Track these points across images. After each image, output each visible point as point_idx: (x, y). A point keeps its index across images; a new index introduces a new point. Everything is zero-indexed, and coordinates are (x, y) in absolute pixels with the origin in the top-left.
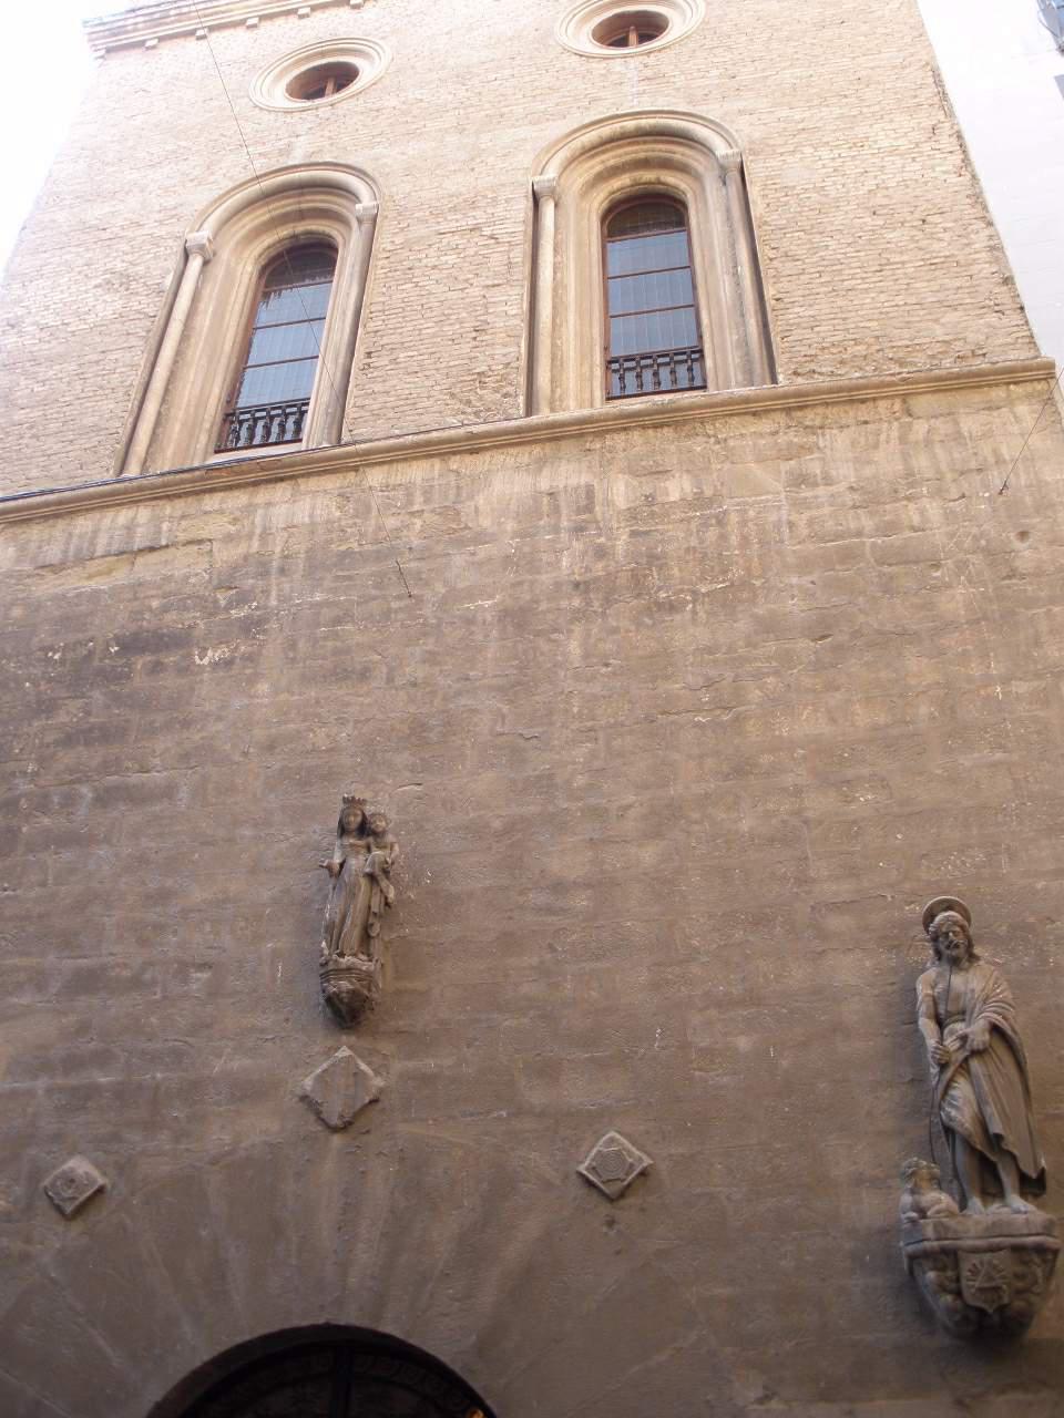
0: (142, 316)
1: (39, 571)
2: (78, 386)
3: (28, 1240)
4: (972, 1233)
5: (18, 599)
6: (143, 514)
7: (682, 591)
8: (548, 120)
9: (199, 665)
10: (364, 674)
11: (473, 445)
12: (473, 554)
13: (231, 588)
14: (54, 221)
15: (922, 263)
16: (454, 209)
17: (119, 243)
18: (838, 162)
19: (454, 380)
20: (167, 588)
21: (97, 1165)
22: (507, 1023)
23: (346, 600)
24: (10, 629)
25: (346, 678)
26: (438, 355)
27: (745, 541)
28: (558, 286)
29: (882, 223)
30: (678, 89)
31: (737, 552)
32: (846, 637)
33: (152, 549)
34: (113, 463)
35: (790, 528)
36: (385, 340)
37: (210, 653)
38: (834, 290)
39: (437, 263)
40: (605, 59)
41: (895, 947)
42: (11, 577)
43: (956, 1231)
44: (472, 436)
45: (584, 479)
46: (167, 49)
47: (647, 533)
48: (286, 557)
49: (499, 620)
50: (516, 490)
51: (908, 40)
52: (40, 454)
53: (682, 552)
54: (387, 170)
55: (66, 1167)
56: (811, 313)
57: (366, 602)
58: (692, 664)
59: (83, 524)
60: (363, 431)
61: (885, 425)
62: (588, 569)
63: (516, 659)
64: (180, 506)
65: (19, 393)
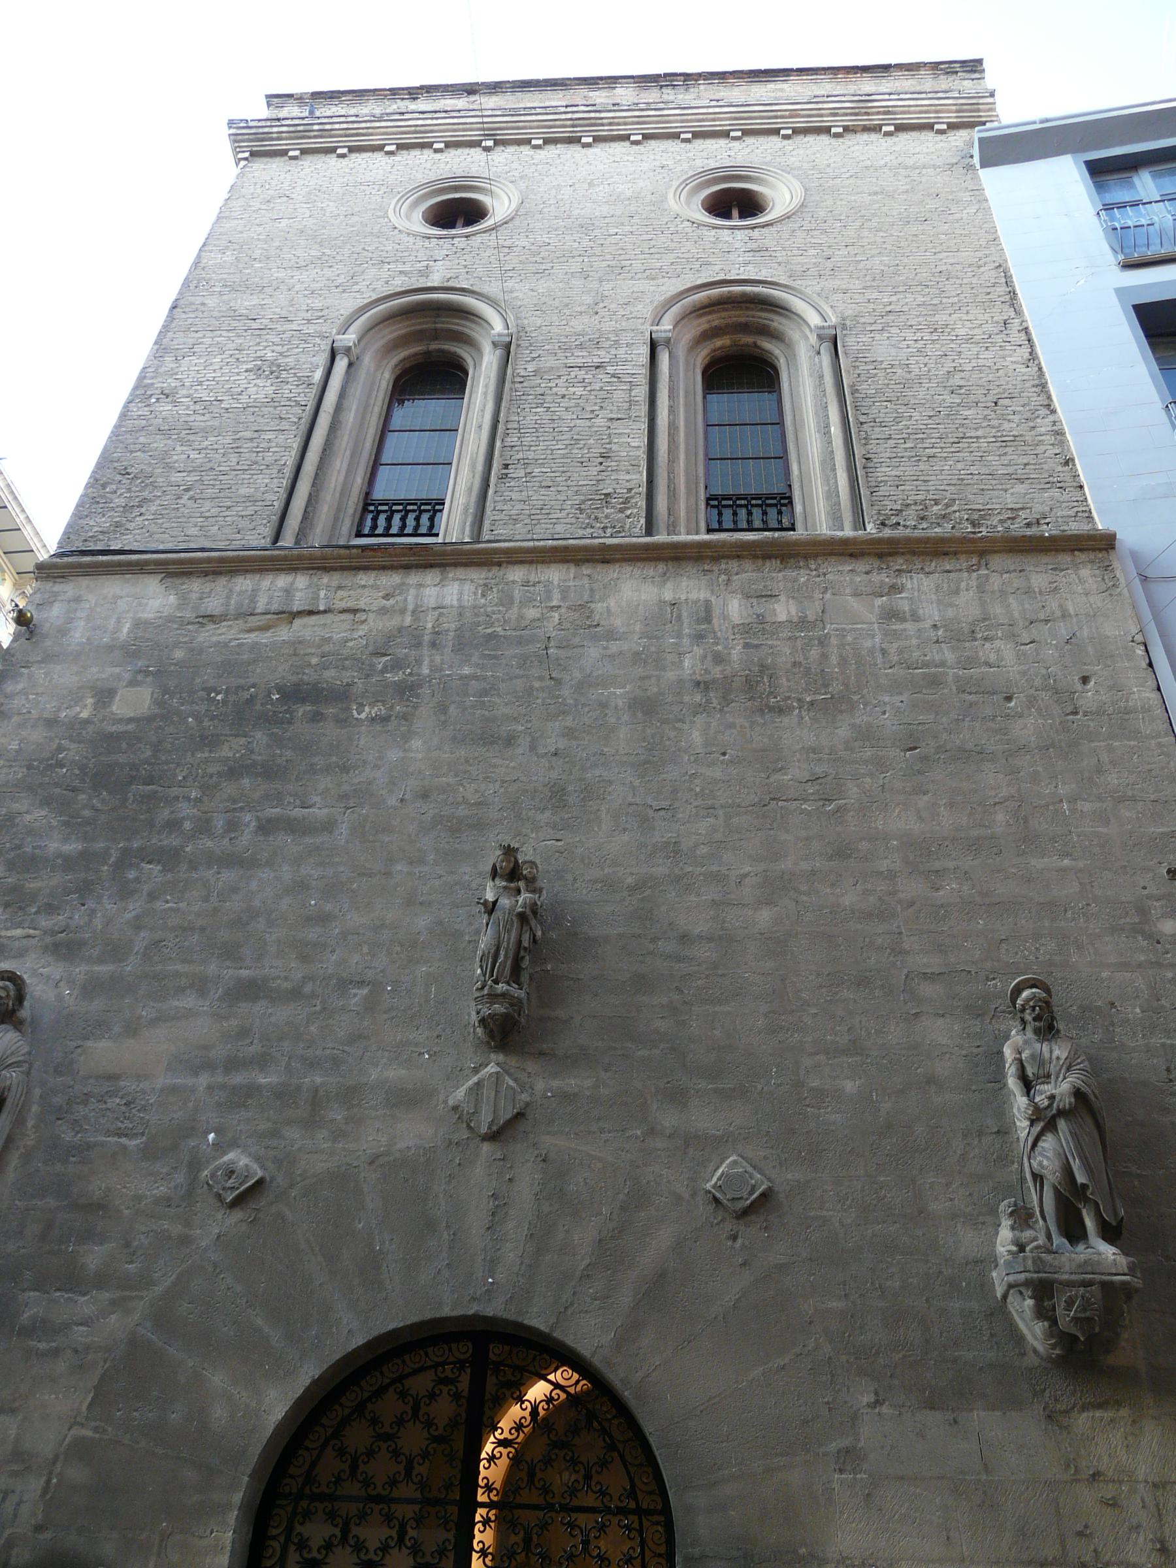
0: (293, 404)
1: (200, 620)
2: (234, 459)
3: (188, 1224)
4: (1067, 1268)
5: (180, 643)
6: (301, 581)
7: (789, 698)
8: (664, 277)
9: (357, 719)
10: (510, 741)
11: (604, 556)
12: (605, 648)
13: (386, 655)
14: (203, 304)
15: (994, 440)
16: (581, 346)
17: (268, 334)
18: (920, 344)
19: (583, 498)
20: (326, 648)
21: (258, 1159)
22: (639, 1053)
23: (492, 676)
24: (172, 668)
25: (492, 743)
26: (568, 474)
27: (843, 662)
28: (673, 427)
29: (958, 401)
30: (779, 264)
31: (836, 670)
32: (933, 751)
33: (311, 613)
34: (268, 531)
35: (883, 654)
36: (520, 456)
37: (367, 709)
38: (916, 456)
39: (566, 393)
40: (714, 228)
41: (980, 1015)
42: (174, 622)
43: (1051, 1266)
44: (604, 548)
45: (703, 595)
46: (308, 163)
47: (757, 646)
48: (437, 633)
49: (630, 707)
50: (643, 598)
51: (983, 242)
52: (199, 515)
53: (789, 666)
54: (519, 303)
55: (226, 1158)
56: (898, 473)
57: (511, 679)
58: (799, 761)
59: (244, 583)
60: (501, 531)
61: (966, 574)
62: (707, 671)
63: (644, 742)
64: (336, 578)
65: (175, 457)
